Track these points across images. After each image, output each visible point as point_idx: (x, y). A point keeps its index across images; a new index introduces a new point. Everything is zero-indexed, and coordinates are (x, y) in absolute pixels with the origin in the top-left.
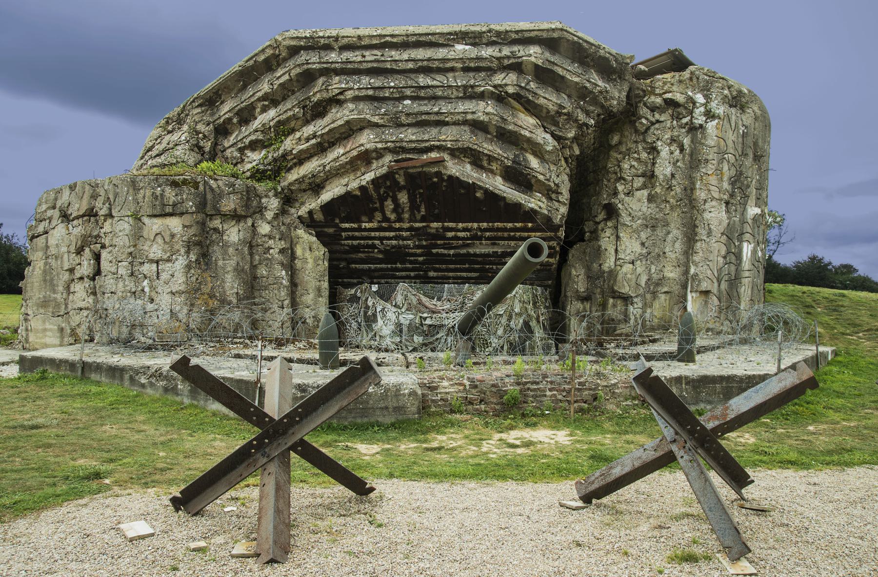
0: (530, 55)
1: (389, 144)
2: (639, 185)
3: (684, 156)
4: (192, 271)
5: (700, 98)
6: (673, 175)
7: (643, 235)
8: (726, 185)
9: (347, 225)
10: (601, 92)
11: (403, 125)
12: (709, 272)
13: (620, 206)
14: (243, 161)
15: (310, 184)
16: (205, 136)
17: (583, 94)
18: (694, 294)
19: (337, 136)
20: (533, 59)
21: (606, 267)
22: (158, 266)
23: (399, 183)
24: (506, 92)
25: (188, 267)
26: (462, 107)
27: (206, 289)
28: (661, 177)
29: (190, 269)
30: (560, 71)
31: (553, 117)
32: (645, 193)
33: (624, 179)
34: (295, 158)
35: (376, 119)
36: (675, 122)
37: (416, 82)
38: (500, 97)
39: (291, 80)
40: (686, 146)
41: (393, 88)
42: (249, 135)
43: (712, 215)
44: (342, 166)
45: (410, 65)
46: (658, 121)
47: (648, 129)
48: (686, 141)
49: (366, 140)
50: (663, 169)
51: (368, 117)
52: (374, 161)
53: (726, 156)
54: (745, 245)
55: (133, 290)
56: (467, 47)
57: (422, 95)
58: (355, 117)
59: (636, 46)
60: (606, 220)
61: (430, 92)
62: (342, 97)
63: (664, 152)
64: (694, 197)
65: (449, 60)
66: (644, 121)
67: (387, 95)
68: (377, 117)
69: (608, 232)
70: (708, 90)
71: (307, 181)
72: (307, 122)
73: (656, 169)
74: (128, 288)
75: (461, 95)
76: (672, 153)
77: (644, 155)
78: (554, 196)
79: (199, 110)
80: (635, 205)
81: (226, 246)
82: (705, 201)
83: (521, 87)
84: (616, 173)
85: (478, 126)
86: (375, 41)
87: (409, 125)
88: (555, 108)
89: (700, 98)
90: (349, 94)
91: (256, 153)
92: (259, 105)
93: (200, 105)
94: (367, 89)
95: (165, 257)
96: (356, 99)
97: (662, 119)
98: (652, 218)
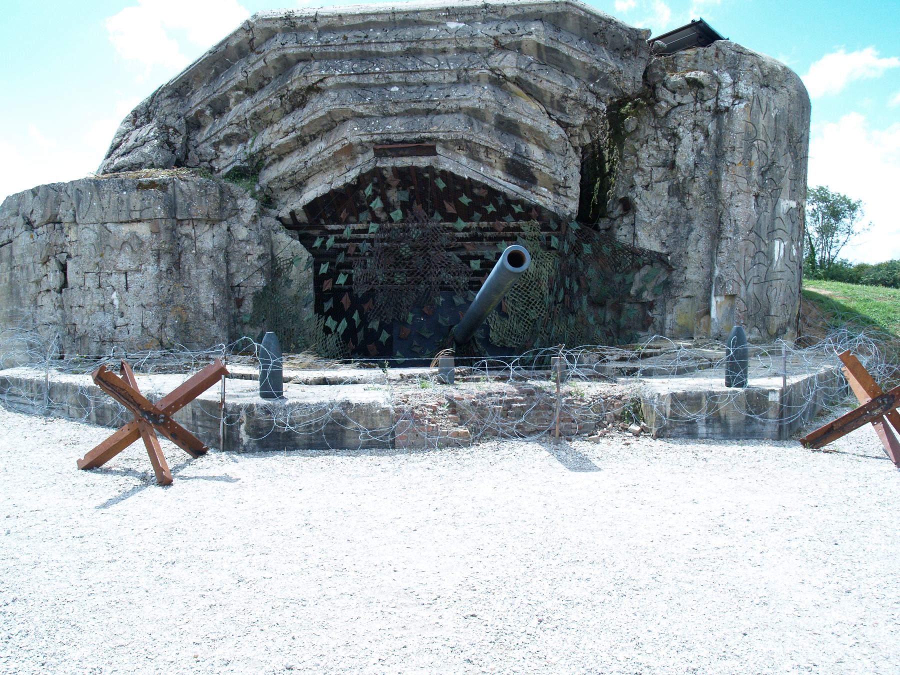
0: (530, 33)
1: (375, 137)
2: (659, 176)
4: (163, 282)
5: (727, 78)
8: (755, 175)
10: (613, 73)
11: (391, 115)
12: (735, 274)
13: (637, 200)
14: (218, 157)
15: (292, 182)
18: (718, 299)
20: (533, 37)
24: (504, 76)
25: (159, 277)
26: (455, 93)
28: (683, 167)
29: (161, 279)
33: (642, 170)
35: (360, 109)
38: (498, 81)
40: (711, 132)
41: (378, 73)
44: (326, 162)
46: (680, 104)
48: (711, 127)
49: (351, 133)
50: (685, 157)
51: (352, 107)
52: (360, 156)
53: (755, 143)
54: (777, 243)
55: (102, 303)
56: (461, 25)
58: (337, 107)
61: (420, 77)
62: (320, 85)
63: (687, 139)
67: (372, 81)
68: (361, 107)
70: (736, 68)
74: (96, 301)
75: (455, 79)
77: (664, 143)
78: (561, 191)
81: (198, 255)
82: (732, 195)
83: (521, 69)
85: (475, 115)
86: (358, 21)
87: (396, 115)
88: (561, 92)
89: (727, 78)
90: (330, 82)
91: (233, 148)
93: (169, 97)
95: (133, 267)
96: (339, 87)
97: (684, 102)
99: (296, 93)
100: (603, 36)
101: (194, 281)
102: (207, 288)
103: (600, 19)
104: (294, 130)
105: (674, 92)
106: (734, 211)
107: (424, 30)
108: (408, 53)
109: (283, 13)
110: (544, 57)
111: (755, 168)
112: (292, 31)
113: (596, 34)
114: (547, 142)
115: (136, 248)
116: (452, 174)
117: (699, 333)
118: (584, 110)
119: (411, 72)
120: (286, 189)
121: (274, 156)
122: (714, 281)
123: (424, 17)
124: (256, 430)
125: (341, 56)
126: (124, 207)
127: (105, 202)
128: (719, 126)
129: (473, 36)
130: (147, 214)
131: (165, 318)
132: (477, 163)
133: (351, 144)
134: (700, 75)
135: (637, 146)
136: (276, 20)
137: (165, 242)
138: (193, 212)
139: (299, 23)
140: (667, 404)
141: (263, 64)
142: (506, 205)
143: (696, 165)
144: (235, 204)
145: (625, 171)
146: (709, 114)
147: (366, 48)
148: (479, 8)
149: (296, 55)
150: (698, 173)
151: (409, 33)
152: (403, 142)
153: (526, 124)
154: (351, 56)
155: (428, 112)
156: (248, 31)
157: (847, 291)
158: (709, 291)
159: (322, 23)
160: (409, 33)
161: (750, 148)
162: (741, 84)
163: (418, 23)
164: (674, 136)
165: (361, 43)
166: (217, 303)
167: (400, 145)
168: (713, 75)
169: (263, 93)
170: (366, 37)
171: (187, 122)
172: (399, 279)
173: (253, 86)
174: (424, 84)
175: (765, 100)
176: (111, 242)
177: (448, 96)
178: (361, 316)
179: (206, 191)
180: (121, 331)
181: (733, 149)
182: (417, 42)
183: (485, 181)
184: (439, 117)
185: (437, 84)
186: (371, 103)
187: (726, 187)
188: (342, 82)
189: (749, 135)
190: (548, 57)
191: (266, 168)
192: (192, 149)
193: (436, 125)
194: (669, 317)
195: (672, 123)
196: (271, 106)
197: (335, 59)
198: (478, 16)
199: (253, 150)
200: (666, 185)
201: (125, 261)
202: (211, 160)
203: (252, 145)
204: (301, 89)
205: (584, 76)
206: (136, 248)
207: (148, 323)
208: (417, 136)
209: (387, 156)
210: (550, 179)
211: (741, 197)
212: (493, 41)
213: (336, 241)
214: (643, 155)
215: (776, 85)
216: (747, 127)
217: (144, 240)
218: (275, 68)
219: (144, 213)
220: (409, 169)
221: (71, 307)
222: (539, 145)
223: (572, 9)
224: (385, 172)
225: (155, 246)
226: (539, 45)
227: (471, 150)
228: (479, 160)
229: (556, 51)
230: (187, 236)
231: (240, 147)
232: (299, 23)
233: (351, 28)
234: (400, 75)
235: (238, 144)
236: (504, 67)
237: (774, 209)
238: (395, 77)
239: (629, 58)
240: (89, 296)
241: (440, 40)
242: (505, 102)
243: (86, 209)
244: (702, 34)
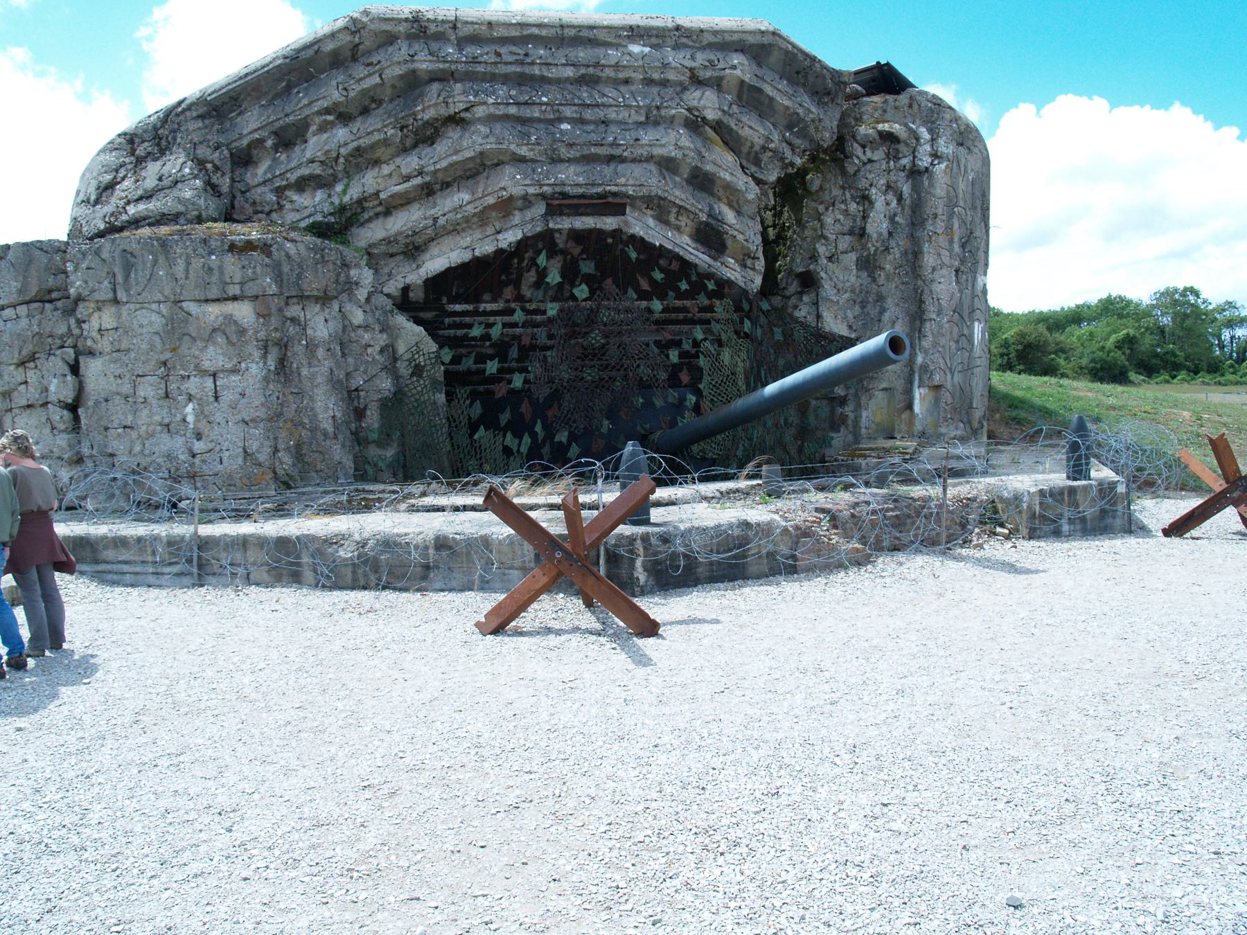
0: (734, 67)
1: (545, 188)
3: (903, 209)
4: (271, 386)
5: (924, 134)
8: (956, 247)
9: (458, 307)
10: (813, 121)
11: (561, 161)
12: (941, 361)
13: (823, 274)
14: (281, 207)
15: (407, 245)
16: (217, 168)
17: (793, 123)
18: (922, 390)
19: (459, 173)
20: (738, 72)
23: (556, 245)
24: (704, 119)
25: (266, 379)
26: (647, 136)
27: (290, 412)
28: (875, 235)
29: (268, 382)
33: (826, 238)
34: (381, 204)
35: (523, 151)
37: (579, 98)
38: (695, 124)
41: (546, 104)
42: (299, 167)
43: (941, 286)
44: (467, 220)
46: (870, 161)
47: (858, 171)
48: (906, 189)
49: (511, 182)
50: (877, 224)
51: (513, 147)
52: (517, 212)
54: (976, 324)
55: (166, 421)
56: (647, 50)
58: (494, 146)
59: (845, 55)
61: (600, 113)
63: (879, 204)
66: (856, 161)
67: (537, 115)
68: (525, 148)
70: (933, 122)
71: (402, 240)
72: (404, 150)
73: (868, 225)
74: (157, 418)
75: (643, 119)
76: (888, 204)
77: (853, 207)
78: (749, 262)
81: (311, 347)
82: (934, 269)
83: (723, 111)
84: (815, 230)
85: (668, 165)
87: (569, 161)
88: (761, 142)
89: (924, 134)
90: (480, 111)
91: (307, 195)
92: (317, 120)
93: (201, 117)
95: (229, 366)
96: (491, 119)
97: (875, 158)
99: (427, 124)
100: (806, 77)
101: (307, 385)
102: (325, 394)
103: (807, 55)
104: (420, 173)
105: (864, 147)
106: (936, 288)
107: (600, 51)
108: (582, 81)
109: (407, 11)
110: (745, 97)
111: (956, 239)
112: (420, 38)
113: (798, 73)
114: (741, 202)
115: (234, 338)
116: (642, 239)
117: (900, 431)
118: (779, 164)
119: (588, 106)
120: (392, 256)
121: (379, 209)
122: (916, 369)
123: (602, 36)
125: (492, 78)
126: (214, 279)
127: (180, 268)
128: (916, 189)
129: (665, 66)
130: (252, 289)
131: (276, 439)
132: (663, 226)
133: (511, 198)
134: (896, 128)
135: (821, 208)
136: (399, 21)
137: (276, 329)
138: (305, 286)
139: (433, 28)
140: (1037, 500)
141: (378, 80)
142: (699, 281)
143: (890, 234)
144: (348, 277)
145: (804, 239)
146: (903, 174)
147: (527, 70)
148: (670, 30)
149: (430, 72)
150: (893, 243)
151: (582, 54)
152: (583, 196)
153: (724, 180)
154: (506, 79)
155: (611, 159)
156: (353, 33)
158: (911, 383)
159: (464, 31)
160: (582, 54)
161: (951, 215)
162: (941, 141)
163: (593, 42)
164: (865, 199)
165: (522, 63)
166: (338, 415)
167: (575, 201)
168: (910, 129)
169: (370, 120)
170: (526, 55)
171: (231, 154)
172: (589, 375)
173: (353, 110)
174: (603, 122)
175: (963, 160)
176: (192, 330)
177: (637, 140)
178: (544, 427)
179: (323, 257)
180: (204, 461)
181: (935, 216)
182: (595, 67)
183: (677, 250)
184: (624, 165)
185: (619, 123)
186: (538, 144)
187: (929, 260)
188: (497, 112)
189: (950, 200)
190: (750, 97)
191: (362, 225)
192: (238, 194)
193: (624, 176)
194: (864, 414)
195: (863, 184)
196: (385, 140)
197: (483, 80)
198: (668, 40)
199: (346, 199)
200: (853, 257)
201: (214, 357)
202: (271, 211)
203: (344, 192)
204: (437, 119)
205: (783, 122)
206: (234, 338)
207: (254, 446)
208: (600, 190)
209: (561, 214)
210: (743, 247)
211: (944, 272)
212: (688, 74)
213: (505, 325)
214: (829, 220)
215: (970, 143)
216: (948, 192)
217: (246, 326)
218: (394, 87)
219: (246, 287)
220: (591, 232)
221: (106, 429)
222: (730, 206)
223: (780, 41)
224: (557, 235)
225: (262, 335)
226: (742, 82)
227: (660, 208)
228: (666, 223)
229: (760, 91)
230: (293, 320)
231: (320, 195)
232: (433, 28)
233: (504, 41)
234: (574, 108)
235: (315, 190)
236: (705, 108)
237: (973, 285)
238: (568, 112)
239: (826, 104)
240: (145, 412)
241: (624, 67)
242: (703, 150)
243: (143, 281)
244: (885, 80)
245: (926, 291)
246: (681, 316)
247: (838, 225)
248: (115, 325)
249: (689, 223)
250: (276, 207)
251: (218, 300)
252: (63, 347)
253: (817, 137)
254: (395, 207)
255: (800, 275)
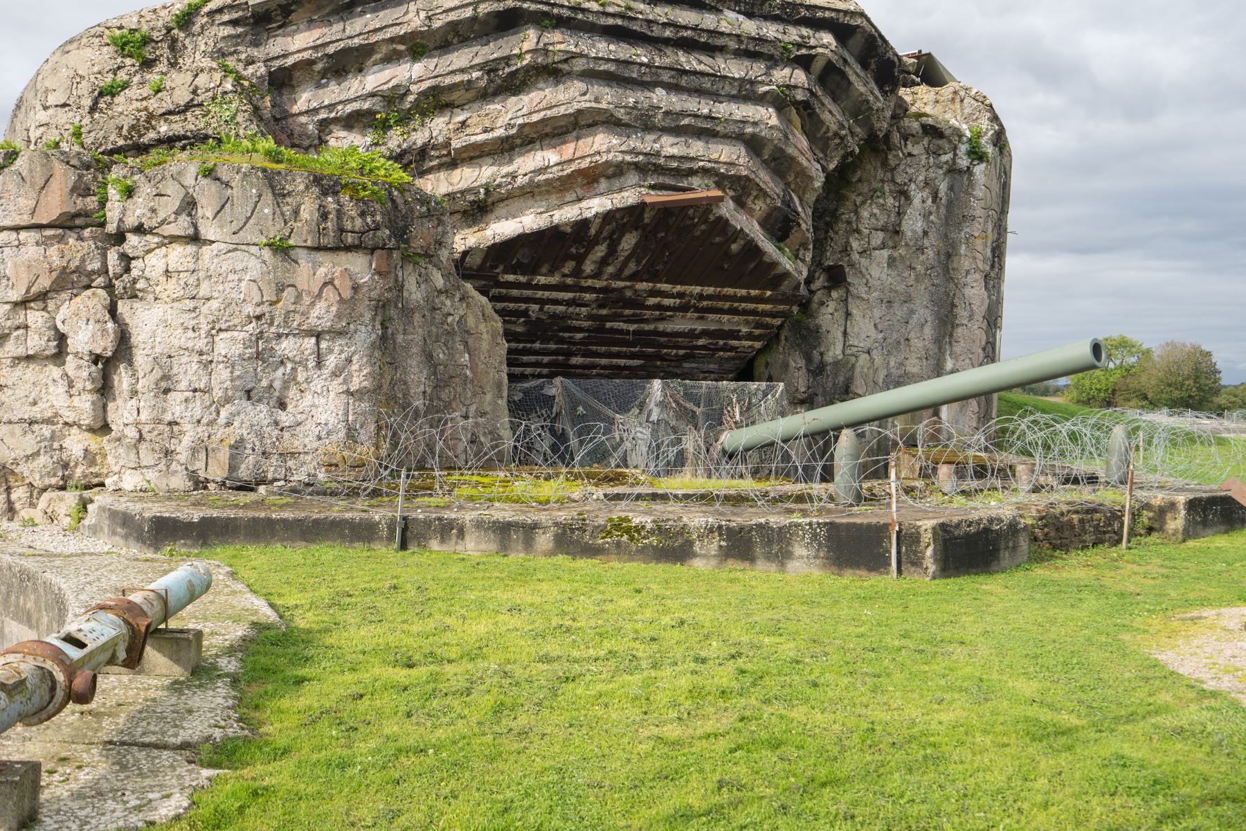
6: (925, 233)
7: (877, 313)
9: (511, 278)
21: (829, 358)
22: (318, 343)
28: (909, 234)
30: (853, 78)
31: (828, 138)
32: (885, 253)
36: (932, 159)
38: (780, 101)
39: (474, 19)
40: (942, 194)
43: (973, 291)
45: (668, 33)
46: (910, 155)
48: (943, 187)
49: (602, 145)
50: (913, 224)
55: (249, 386)
57: (683, 83)
58: (588, 105)
60: (829, 289)
61: (695, 81)
62: (565, 67)
63: (918, 197)
64: (955, 265)
65: (722, 34)
67: (635, 75)
68: (622, 111)
69: (832, 306)
75: (734, 92)
79: (229, 30)
80: (875, 271)
82: (968, 272)
85: (754, 144)
90: (579, 64)
93: (234, 23)
94: (609, 60)
97: (915, 152)
98: (891, 290)
106: (968, 291)
124: (668, 499)
135: (859, 200)
157: (859, 591)
225: (374, 294)
245: (959, 295)
246: (727, 305)
247: (873, 220)
248: (191, 266)
249: (764, 207)
250: (316, 142)
251: (331, 249)
252: (88, 287)
253: (877, 125)
254: (463, 160)
255: (829, 270)
